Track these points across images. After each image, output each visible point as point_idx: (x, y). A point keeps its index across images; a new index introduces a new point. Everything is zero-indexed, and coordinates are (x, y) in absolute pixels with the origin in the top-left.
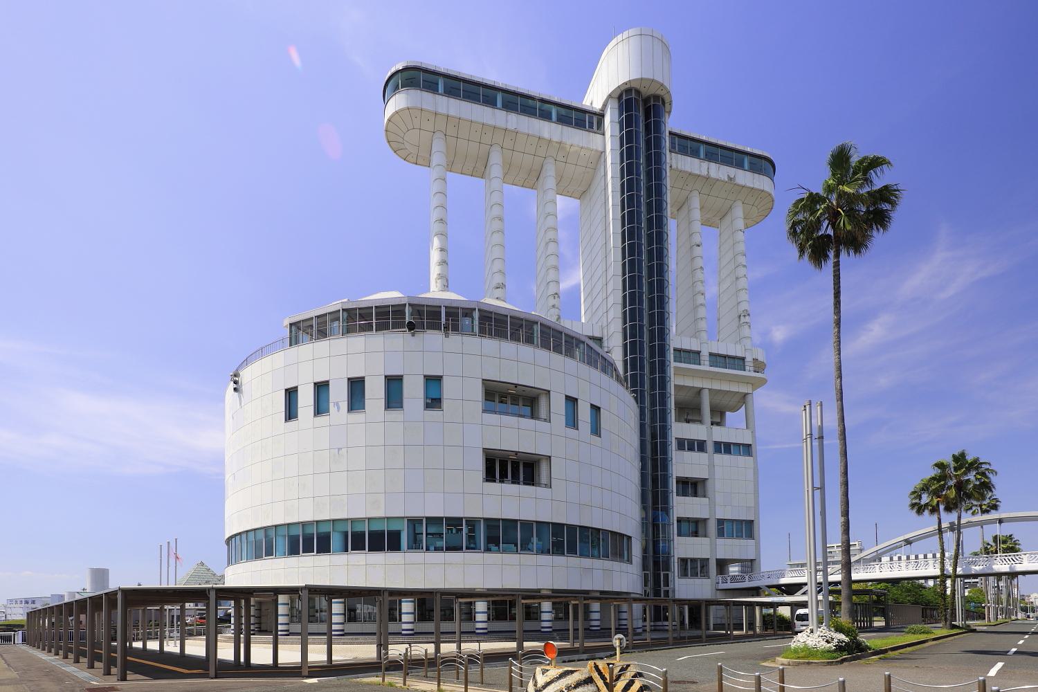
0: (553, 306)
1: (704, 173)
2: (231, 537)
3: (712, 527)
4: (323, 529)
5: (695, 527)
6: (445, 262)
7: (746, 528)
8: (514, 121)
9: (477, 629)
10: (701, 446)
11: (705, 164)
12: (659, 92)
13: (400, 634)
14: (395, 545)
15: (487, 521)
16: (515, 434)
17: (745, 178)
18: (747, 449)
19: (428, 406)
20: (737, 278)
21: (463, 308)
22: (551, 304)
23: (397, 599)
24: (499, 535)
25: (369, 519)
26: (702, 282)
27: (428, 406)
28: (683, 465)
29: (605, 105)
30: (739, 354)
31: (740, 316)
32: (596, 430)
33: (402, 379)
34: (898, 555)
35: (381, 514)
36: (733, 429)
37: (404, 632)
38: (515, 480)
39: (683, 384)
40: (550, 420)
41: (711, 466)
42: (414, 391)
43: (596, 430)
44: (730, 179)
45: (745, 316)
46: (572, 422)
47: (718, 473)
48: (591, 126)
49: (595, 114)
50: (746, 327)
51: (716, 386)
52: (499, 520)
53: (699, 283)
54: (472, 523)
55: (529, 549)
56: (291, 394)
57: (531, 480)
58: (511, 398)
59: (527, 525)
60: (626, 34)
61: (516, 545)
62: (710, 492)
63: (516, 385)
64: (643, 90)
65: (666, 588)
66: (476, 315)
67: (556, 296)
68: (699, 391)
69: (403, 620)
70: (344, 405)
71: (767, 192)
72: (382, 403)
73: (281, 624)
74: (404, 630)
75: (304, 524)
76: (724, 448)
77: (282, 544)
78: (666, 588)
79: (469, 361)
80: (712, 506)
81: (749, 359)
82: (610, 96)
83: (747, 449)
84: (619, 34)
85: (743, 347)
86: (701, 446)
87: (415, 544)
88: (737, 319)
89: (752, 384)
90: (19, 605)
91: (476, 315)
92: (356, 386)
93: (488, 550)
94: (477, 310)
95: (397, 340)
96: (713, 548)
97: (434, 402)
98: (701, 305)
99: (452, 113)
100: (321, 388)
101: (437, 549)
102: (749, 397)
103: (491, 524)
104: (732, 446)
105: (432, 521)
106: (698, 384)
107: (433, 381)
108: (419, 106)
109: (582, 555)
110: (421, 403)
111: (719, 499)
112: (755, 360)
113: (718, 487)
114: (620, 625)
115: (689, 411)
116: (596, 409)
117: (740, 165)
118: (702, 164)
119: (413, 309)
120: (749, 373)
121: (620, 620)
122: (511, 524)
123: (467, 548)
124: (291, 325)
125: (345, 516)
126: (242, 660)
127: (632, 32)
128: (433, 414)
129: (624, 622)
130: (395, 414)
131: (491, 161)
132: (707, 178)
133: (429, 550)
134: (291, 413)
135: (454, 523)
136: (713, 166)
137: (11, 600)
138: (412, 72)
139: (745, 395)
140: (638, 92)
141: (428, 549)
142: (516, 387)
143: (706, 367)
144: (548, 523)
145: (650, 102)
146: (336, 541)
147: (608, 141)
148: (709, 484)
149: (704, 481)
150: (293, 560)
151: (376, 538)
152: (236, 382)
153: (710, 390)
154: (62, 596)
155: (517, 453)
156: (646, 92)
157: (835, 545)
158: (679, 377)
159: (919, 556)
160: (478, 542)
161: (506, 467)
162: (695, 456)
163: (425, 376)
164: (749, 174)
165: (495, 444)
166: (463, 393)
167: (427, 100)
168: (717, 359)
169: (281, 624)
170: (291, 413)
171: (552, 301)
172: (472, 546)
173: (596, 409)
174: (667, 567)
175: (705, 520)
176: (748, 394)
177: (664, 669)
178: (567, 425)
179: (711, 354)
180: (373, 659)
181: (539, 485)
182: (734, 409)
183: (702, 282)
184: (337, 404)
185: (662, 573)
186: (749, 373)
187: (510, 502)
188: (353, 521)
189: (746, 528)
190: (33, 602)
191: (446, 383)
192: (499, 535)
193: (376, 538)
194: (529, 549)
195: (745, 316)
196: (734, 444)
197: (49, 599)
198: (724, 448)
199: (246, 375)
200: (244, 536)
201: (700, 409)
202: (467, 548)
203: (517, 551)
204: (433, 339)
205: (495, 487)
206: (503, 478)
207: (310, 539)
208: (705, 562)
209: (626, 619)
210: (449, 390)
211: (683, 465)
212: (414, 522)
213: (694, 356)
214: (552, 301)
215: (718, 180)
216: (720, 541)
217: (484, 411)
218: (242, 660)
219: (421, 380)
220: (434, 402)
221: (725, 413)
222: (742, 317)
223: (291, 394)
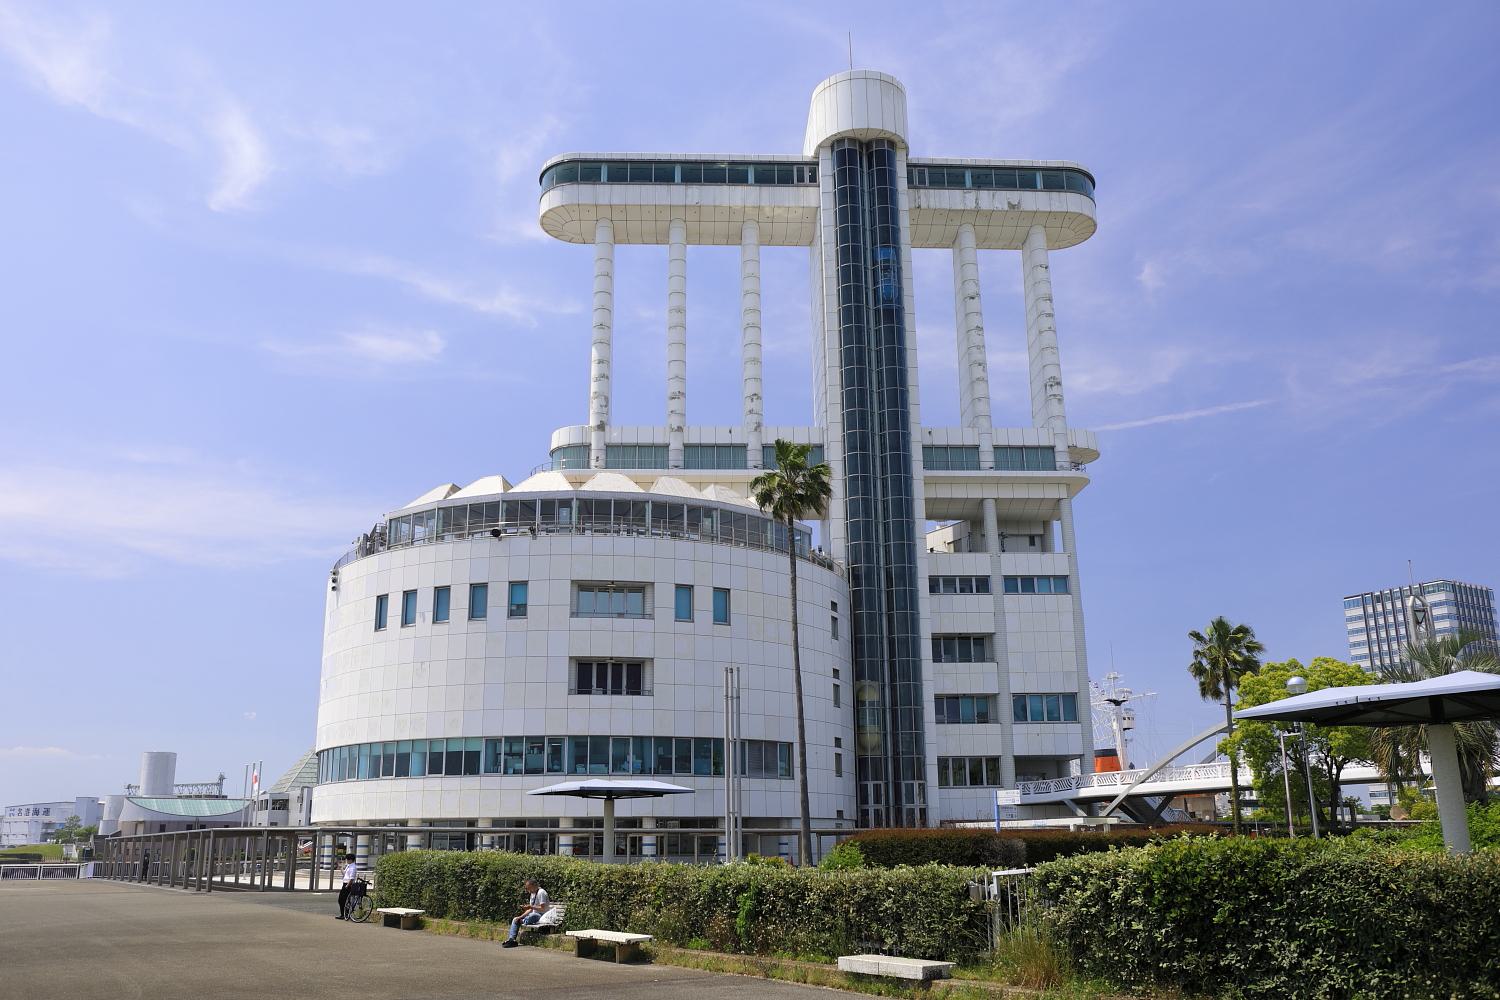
0: (751, 412)
1: (971, 205)
2: (320, 752)
3: (1006, 707)
4: (404, 749)
6: (603, 376)
7: (1065, 707)
8: (696, 194)
10: (983, 585)
11: (971, 196)
14: (472, 769)
16: (610, 639)
19: (512, 614)
20: (1041, 332)
22: (749, 408)
23: (405, 834)
24: (589, 752)
25: (447, 739)
26: (978, 347)
27: (512, 614)
29: (817, 155)
30: (1044, 442)
35: (458, 733)
39: (949, 496)
41: (999, 614)
42: (498, 600)
44: (1012, 206)
45: (1051, 385)
47: (1012, 623)
48: (801, 179)
49: (806, 164)
50: (1054, 401)
51: (1006, 493)
52: (587, 736)
53: (974, 349)
54: (556, 742)
55: (624, 770)
56: (382, 600)
57: (635, 688)
59: (622, 741)
60: (833, 79)
61: (607, 764)
62: (999, 655)
63: (613, 582)
65: (909, 806)
66: (575, 504)
67: (755, 397)
69: (644, 853)
70: (430, 616)
72: (466, 613)
73: (359, 857)
75: (385, 744)
76: (1024, 584)
77: (365, 764)
78: (909, 806)
79: (556, 560)
80: (1003, 674)
81: (1060, 447)
84: (554, 431)
85: (1051, 430)
87: (493, 768)
90: (24, 818)
91: (575, 504)
92: (442, 594)
97: (518, 610)
98: (978, 379)
99: (615, 201)
100: (478, 591)
103: (578, 742)
104: (1035, 580)
106: (975, 493)
107: (518, 587)
108: (576, 202)
109: (698, 773)
110: (505, 611)
111: (1014, 663)
112: (1072, 449)
113: (1013, 645)
118: (967, 195)
122: (600, 742)
124: (391, 520)
125: (424, 737)
126: (266, 884)
127: (839, 76)
128: (518, 622)
130: (478, 625)
132: (977, 211)
134: (380, 623)
135: (536, 742)
137: (12, 809)
141: (505, 773)
144: (650, 737)
146: (415, 763)
147: (820, 198)
148: (997, 640)
149: (991, 635)
150: (373, 784)
151: (454, 761)
152: (334, 581)
153: (996, 500)
154: (94, 804)
156: (864, 138)
161: (594, 675)
165: (585, 652)
166: (550, 597)
167: (585, 193)
169: (359, 857)
170: (380, 623)
171: (749, 405)
172: (556, 767)
174: (920, 774)
183: (978, 347)
184: (423, 614)
187: (608, 715)
188: (431, 741)
189: (1065, 707)
190: (47, 812)
193: (454, 761)
194: (624, 770)
195: (1051, 385)
196: (1040, 577)
197: (74, 806)
198: (1024, 584)
199: (345, 573)
200: (326, 753)
207: (392, 761)
208: (994, 761)
210: (534, 597)
212: (492, 742)
213: (964, 456)
214: (749, 405)
218: (266, 884)
220: (518, 610)
223: (382, 600)
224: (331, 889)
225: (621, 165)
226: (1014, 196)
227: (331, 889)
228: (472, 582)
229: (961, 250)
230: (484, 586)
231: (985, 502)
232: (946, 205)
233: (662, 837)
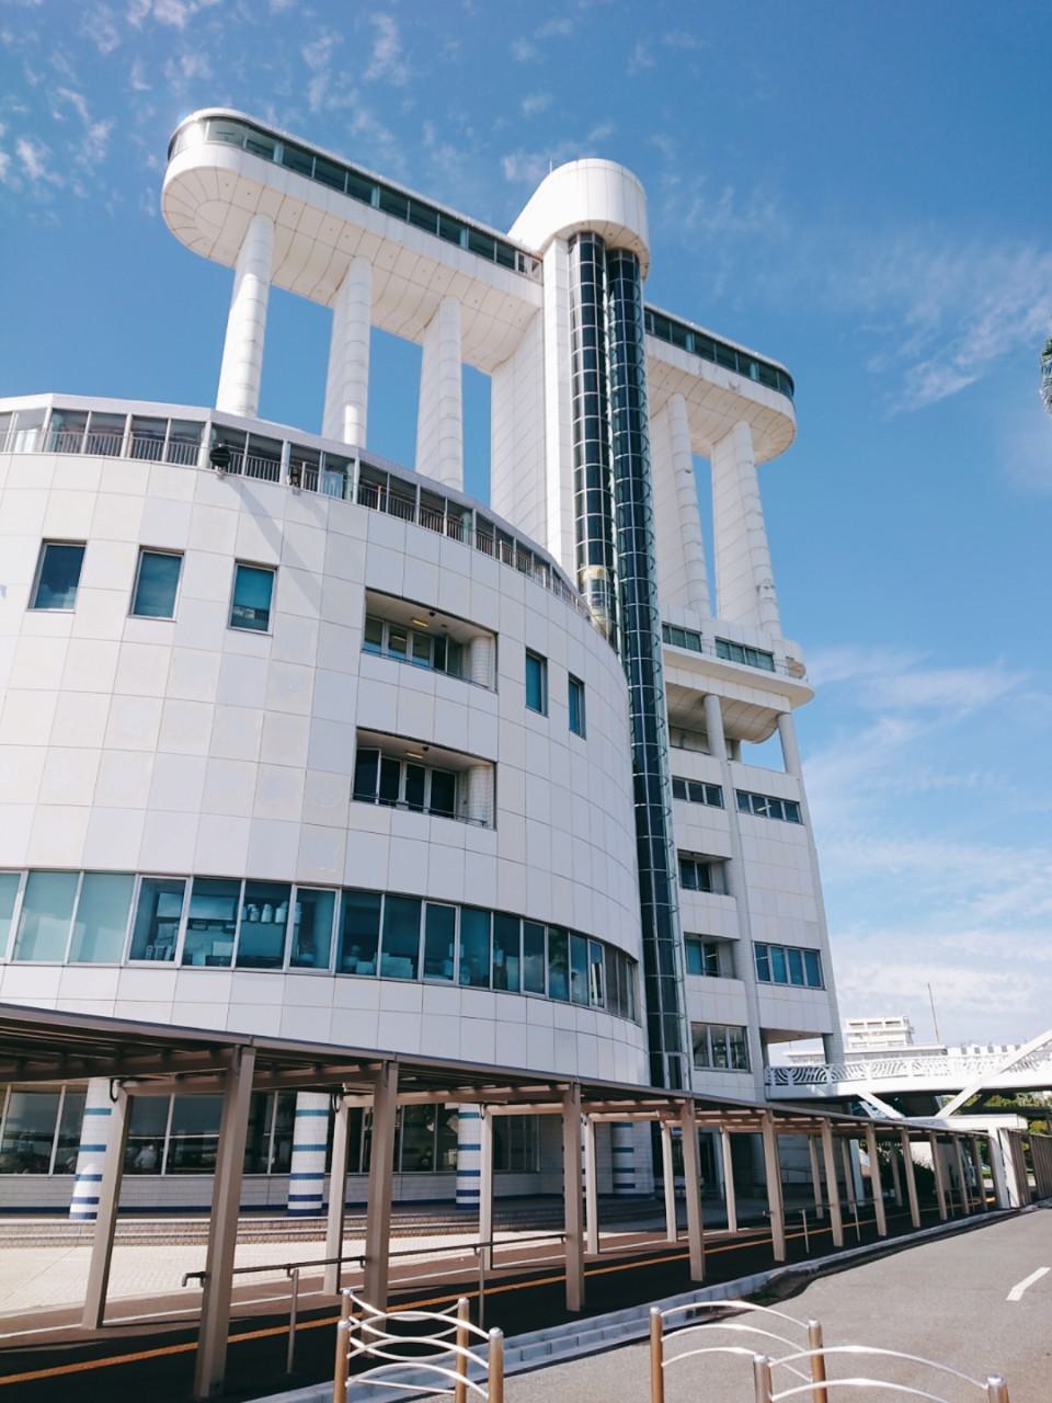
3: (747, 959)
5: (712, 954)
9: (293, 1198)
10: (713, 795)
12: (631, 247)
13: (281, 1209)
15: (350, 893)
16: (420, 707)
17: (752, 389)
18: (788, 810)
19: (236, 622)
21: (328, 455)
24: (380, 931)
27: (236, 622)
28: (689, 827)
29: (546, 247)
31: (758, 588)
32: (577, 724)
33: (180, 559)
34: (974, 1046)
36: (756, 769)
37: (293, 1205)
38: (415, 804)
40: (496, 690)
41: (735, 836)
43: (577, 724)
45: (767, 588)
46: (537, 699)
58: (415, 637)
59: (442, 913)
63: (433, 611)
64: (606, 237)
68: (702, 699)
71: (785, 417)
74: (293, 1198)
80: (743, 913)
81: (779, 657)
82: (556, 236)
83: (788, 810)
86: (713, 795)
88: (755, 592)
89: (790, 699)
93: (344, 969)
94: (357, 464)
95: (197, 480)
96: (752, 1001)
101: (212, 961)
102: (783, 719)
103: (360, 901)
105: (209, 887)
113: (748, 872)
114: (617, 1186)
115: (691, 731)
116: (576, 685)
117: (745, 372)
119: (218, 435)
120: (780, 675)
121: (616, 1170)
123: (294, 963)
128: (246, 640)
129: (627, 1178)
131: (351, 278)
133: (190, 963)
136: (706, 364)
138: (240, 127)
139: (778, 715)
140: (600, 239)
142: (432, 614)
143: (709, 654)
145: (617, 256)
149: (722, 862)
153: (721, 698)
155: (426, 745)
157: (865, 1021)
158: (675, 671)
159: (1008, 1047)
160: (321, 944)
161: (402, 774)
162: (703, 811)
163: (237, 561)
164: (760, 388)
168: (727, 647)
172: (307, 957)
173: (576, 685)
175: (730, 943)
176: (782, 713)
177: (813, 1323)
178: (529, 704)
179: (718, 641)
180: (74, 1314)
181: (467, 819)
182: (758, 738)
185: (666, 1057)
186: (780, 675)
187: (405, 853)
189: (802, 966)
191: (283, 583)
192: (380, 931)
201: (706, 735)
202: (294, 963)
203: (415, 977)
204: (277, 493)
205: (375, 813)
206: (389, 798)
209: (632, 1170)
210: (286, 598)
211: (689, 827)
213: (690, 638)
215: (714, 385)
216: (766, 990)
217: (363, 650)
219: (228, 573)
221: (739, 742)
222: (762, 589)
224: (72, 1200)
225: (303, 156)
226: (735, 378)
227: (72, 1200)
228: (145, 543)
229: (670, 422)
230: (175, 558)
231: (709, 698)
232: (671, 361)
233: (253, 1163)
